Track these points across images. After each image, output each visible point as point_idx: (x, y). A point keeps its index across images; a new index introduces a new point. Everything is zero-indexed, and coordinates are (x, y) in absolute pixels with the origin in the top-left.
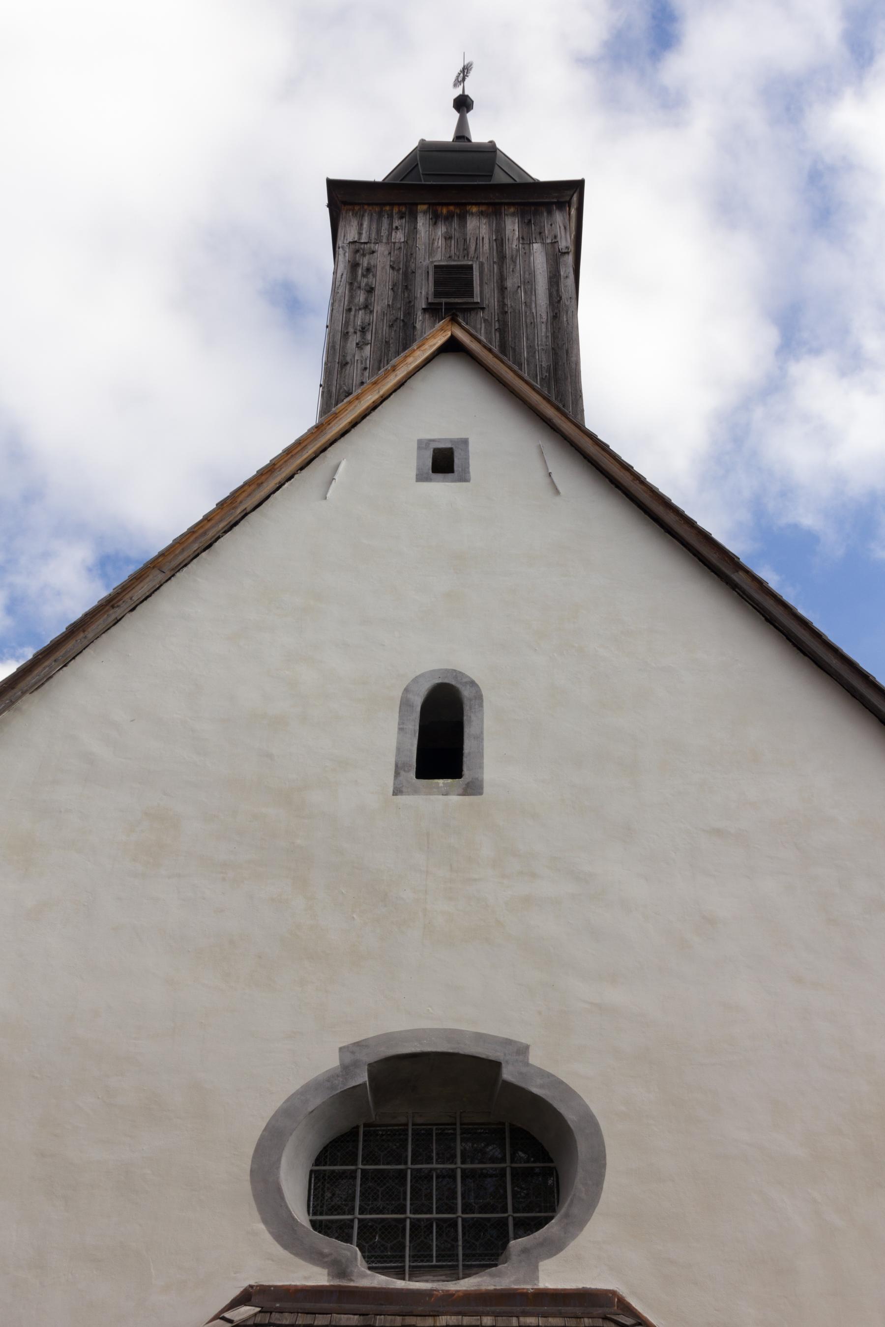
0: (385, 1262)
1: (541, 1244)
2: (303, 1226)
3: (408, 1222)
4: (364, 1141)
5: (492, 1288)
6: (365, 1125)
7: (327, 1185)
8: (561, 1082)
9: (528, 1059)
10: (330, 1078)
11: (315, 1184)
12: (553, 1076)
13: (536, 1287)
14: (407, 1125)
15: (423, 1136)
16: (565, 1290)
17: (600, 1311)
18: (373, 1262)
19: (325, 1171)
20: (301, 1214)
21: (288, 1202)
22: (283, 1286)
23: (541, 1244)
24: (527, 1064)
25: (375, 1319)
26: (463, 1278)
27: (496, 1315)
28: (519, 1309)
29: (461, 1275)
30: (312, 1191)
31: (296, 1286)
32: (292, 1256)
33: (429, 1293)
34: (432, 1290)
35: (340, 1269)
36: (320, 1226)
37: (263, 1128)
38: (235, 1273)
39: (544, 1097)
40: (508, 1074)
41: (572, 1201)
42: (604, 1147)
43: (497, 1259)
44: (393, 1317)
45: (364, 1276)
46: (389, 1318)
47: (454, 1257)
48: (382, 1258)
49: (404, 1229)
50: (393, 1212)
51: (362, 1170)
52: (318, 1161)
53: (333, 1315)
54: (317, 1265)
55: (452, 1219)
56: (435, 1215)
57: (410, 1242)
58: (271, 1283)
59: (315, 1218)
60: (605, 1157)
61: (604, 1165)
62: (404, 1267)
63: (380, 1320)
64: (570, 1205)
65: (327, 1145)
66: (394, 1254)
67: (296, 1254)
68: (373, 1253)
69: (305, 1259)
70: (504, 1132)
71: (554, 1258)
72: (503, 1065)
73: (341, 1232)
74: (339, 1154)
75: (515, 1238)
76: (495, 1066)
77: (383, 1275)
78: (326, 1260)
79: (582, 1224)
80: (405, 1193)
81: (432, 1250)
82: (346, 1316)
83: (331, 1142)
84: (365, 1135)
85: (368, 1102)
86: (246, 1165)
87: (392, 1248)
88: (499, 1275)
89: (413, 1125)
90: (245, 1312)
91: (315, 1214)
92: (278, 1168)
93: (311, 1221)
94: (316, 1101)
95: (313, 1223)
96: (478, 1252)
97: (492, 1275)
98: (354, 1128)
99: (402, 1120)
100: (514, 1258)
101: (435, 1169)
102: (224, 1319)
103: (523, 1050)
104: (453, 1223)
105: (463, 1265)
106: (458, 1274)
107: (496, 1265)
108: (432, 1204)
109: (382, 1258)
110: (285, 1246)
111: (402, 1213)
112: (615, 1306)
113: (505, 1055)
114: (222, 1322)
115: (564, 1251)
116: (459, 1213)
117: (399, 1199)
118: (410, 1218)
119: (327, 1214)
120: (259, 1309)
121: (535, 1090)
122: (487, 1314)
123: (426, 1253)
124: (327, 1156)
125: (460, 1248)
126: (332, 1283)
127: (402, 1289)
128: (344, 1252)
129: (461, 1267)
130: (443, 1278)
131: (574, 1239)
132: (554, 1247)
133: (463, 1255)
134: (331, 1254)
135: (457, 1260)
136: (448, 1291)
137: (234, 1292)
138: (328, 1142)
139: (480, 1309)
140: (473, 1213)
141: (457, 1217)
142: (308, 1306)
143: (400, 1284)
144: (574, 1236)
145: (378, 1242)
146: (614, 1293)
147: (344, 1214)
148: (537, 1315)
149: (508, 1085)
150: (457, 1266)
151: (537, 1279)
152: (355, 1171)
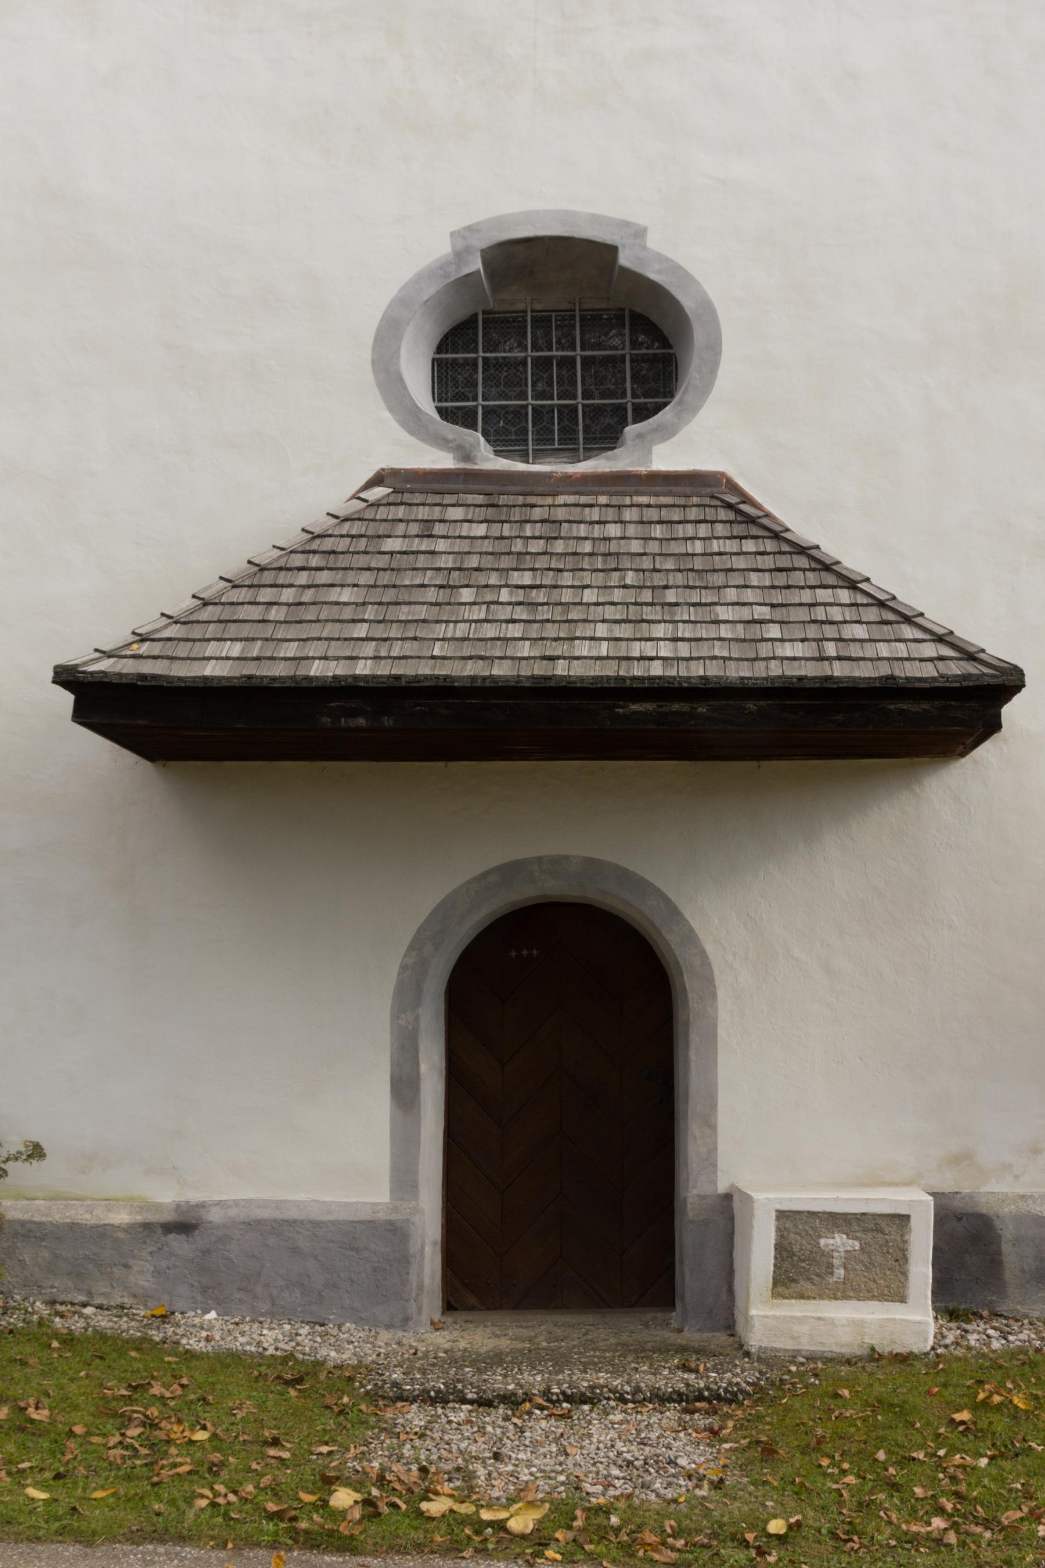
0: (510, 445)
1: (655, 430)
2: (427, 414)
3: (530, 408)
4: (484, 328)
5: (607, 470)
6: (484, 312)
7: (450, 373)
8: (680, 267)
9: (645, 243)
10: (443, 266)
11: (438, 371)
12: (671, 260)
13: (649, 469)
14: (525, 312)
15: (542, 322)
16: (676, 471)
17: (709, 490)
18: (498, 445)
19: (447, 359)
20: (427, 404)
21: (410, 391)
22: (412, 469)
23: (655, 430)
24: (644, 248)
25: (499, 498)
26: (584, 460)
27: (611, 494)
28: (633, 489)
29: (582, 458)
30: (436, 379)
31: (424, 469)
32: (418, 441)
33: (548, 476)
34: (552, 472)
35: (465, 454)
36: (446, 412)
37: (379, 318)
38: (367, 457)
39: (660, 282)
40: (625, 259)
41: (686, 389)
42: (720, 333)
43: (616, 443)
44: (515, 497)
45: (487, 459)
46: (512, 497)
47: (575, 441)
48: (507, 441)
49: (527, 414)
50: (516, 399)
51: (483, 358)
52: (439, 349)
53: (652, 567)
54: (443, 450)
55: (573, 405)
56: (556, 402)
57: (533, 426)
58: (401, 467)
59: (440, 404)
60: (720, 345)
61: (720, 353)
62: (527, 450)
63: (504, 499)
64: (684, 393)
65: (448, 333)
66: (519, 438)
67: (423, 440)
68: (498, 438)
69: (431, 445)
70: (624, 319)
71: (667, 443)
72: (620, 249)
73: (465, 419)
74: (460, 342)
75: (635, 422)
76: (611, 251)
77: (506, 458)
78: (451, 445)
79: (695, 410)
80: (526, 379)
81: (554, 435)
82: (472, 496)
83: (451, 330)
84: (484, 322)
85: (484, 289)
86: (367, 355)
87: (516, 433)
88: (615, 458)
89: (532, 311)
90: (378, 493)
91: (440, 400)
92: (398, 358)
93: (436, 407)
94: (431, 290)
95: (440, 410)
96: (598, 435)
97: (607, 459)
98: (472, 315)
99: (521, 306)
100: (629, 442)
101: (554, 356)
102: (359, 498)
103: (641, 233)
104: (574, 409)
105: (584, 448)
106: (579, 456)
107: (613, 448)
108: (553, 390)
109: (507, 441)
110: (412, 433)
111: (524, 400)
112: (722, 486)
113: (622, 238)
114: (358, 501)
115: (677, 436)
116: (580, 399)
117: (521, 386)
118: (532, 405)
119: (452, 401)
120: (391, 490)
121: (653, 276)
122: (603, 494)
123: (548, 437)
124: (447, 345)
125: (581, 433)
126: (458, 467)
127: (523, 472)
128: (467, 438)
129: (581, 450)
130: (565, 460)
131: (687, 425)
132: (667, 433)
133: (584, 438)
134: (455, 440)
135: (578, 444)
136: (566, 473)
137: (368, 474)
138: (447, 330)
139: (597, 489)
140: (594, 399)
141: (578, 403)
142: (437, 487)
143: (521, 467)
144: (686, 423)
145: (503, 427)
146: (723, 474)
147: (468, 400)
148: (649, 494)
149: (626, 272)
150: (579, 449)
151: (651, 461)
152: (476, 359)
